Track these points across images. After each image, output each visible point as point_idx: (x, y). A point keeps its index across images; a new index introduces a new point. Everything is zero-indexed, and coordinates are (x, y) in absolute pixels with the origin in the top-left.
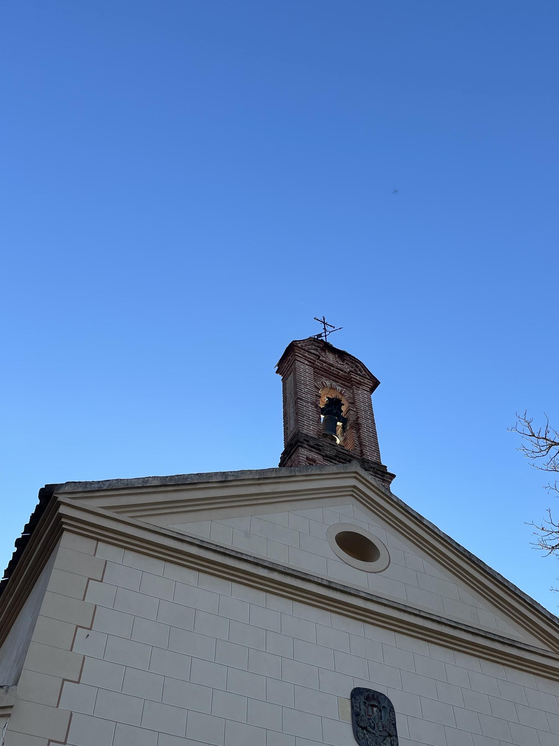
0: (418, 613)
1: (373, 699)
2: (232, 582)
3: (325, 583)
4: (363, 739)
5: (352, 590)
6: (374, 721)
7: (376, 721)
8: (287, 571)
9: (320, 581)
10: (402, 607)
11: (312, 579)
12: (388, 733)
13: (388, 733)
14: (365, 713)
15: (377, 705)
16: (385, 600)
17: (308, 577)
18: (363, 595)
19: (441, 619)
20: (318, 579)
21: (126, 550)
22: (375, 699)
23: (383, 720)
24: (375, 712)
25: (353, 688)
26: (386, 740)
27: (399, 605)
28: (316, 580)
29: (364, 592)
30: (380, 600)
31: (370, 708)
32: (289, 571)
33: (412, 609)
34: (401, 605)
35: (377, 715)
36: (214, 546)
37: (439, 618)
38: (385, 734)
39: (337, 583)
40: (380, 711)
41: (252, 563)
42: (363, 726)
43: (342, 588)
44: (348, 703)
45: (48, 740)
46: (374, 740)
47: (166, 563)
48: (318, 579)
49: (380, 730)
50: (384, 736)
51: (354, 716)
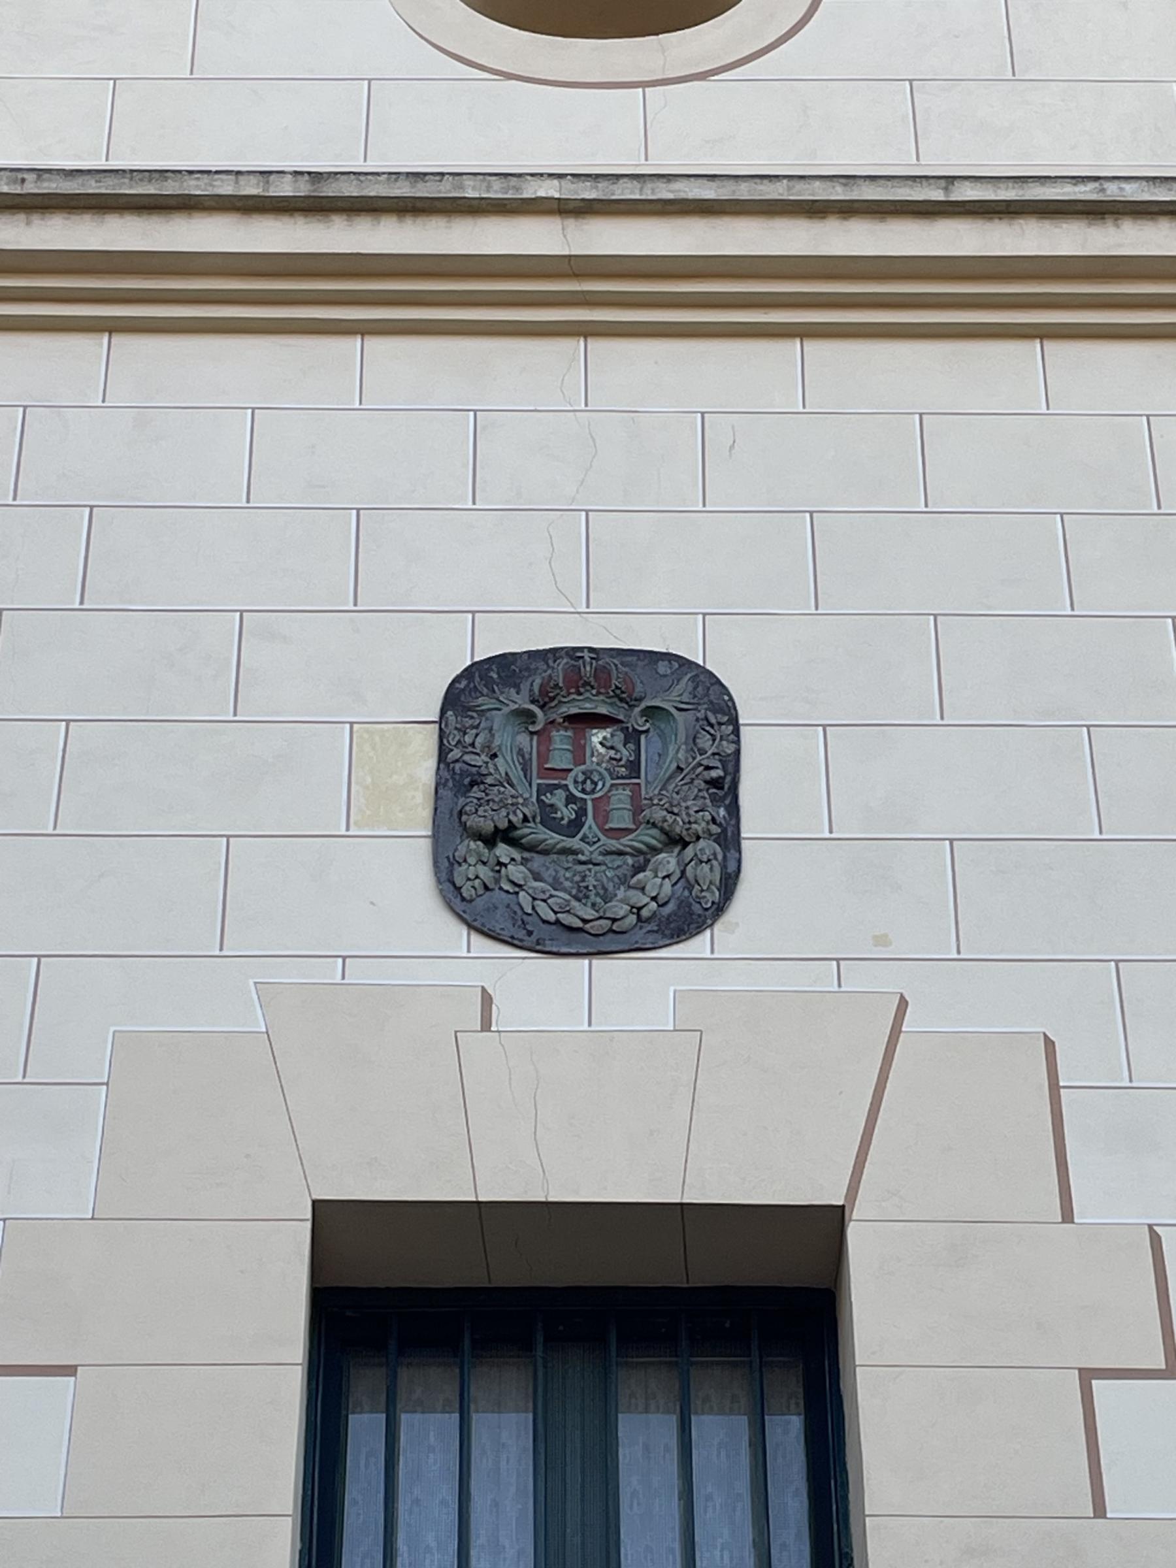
0: (936, 194)
1: (577, 683)
2: (1045, 342)
3: (285, 189)
4: (486, 888)
5: (467, 183)
6: (583, 791)
7: (593, 791)
8: (31, 187)
9: (251, 188)
10: (820, 192)
11: (194, 187)
12: (662, 830)
13: (662, 830)
14: (526, 770)
15: (603, 710)
16: (704, 181)
17: (170, 188)
18: (549, 190)
19: (1103, 190)
20: (241, 178)
21: (1050, 345)
22: (587, 683)
23: (642, 781)
24: (599, 747)
25: (469, 663)
26: (650, 867)
27: (800, 186)
28: (226, 188)
29: (551, 175)
30: (665, 192)
31: (561, 739)
32: (46, 184)
33: (895, 182)
34: (817, 183)
35: (611, 758)
36: (867, 183)
37: (1091, 186)
38: (642, 842)
39: (366, 174)
40: (632, 736)
41: (640, 207)
42: (488, 827)
43: (403, 190)
44: (424, 744)
45: (1076, 1372)
46: (567, 884)
47: (805, 343)
48: (237, 182)
49: (612, 829)
50: (640, 852)
51: (446, 793)
